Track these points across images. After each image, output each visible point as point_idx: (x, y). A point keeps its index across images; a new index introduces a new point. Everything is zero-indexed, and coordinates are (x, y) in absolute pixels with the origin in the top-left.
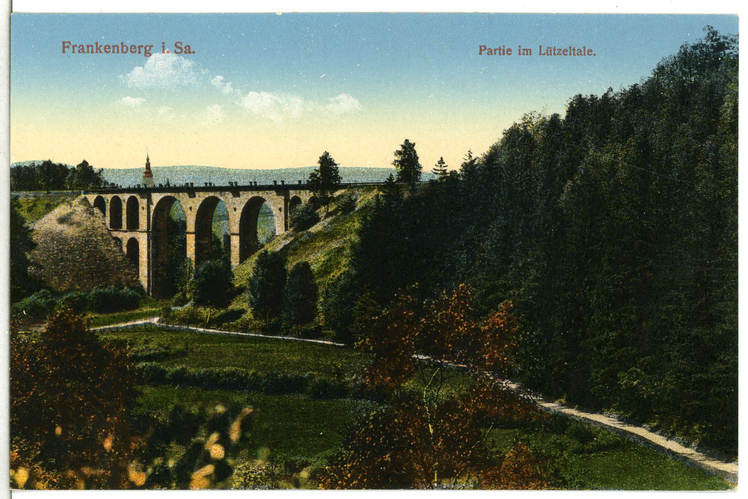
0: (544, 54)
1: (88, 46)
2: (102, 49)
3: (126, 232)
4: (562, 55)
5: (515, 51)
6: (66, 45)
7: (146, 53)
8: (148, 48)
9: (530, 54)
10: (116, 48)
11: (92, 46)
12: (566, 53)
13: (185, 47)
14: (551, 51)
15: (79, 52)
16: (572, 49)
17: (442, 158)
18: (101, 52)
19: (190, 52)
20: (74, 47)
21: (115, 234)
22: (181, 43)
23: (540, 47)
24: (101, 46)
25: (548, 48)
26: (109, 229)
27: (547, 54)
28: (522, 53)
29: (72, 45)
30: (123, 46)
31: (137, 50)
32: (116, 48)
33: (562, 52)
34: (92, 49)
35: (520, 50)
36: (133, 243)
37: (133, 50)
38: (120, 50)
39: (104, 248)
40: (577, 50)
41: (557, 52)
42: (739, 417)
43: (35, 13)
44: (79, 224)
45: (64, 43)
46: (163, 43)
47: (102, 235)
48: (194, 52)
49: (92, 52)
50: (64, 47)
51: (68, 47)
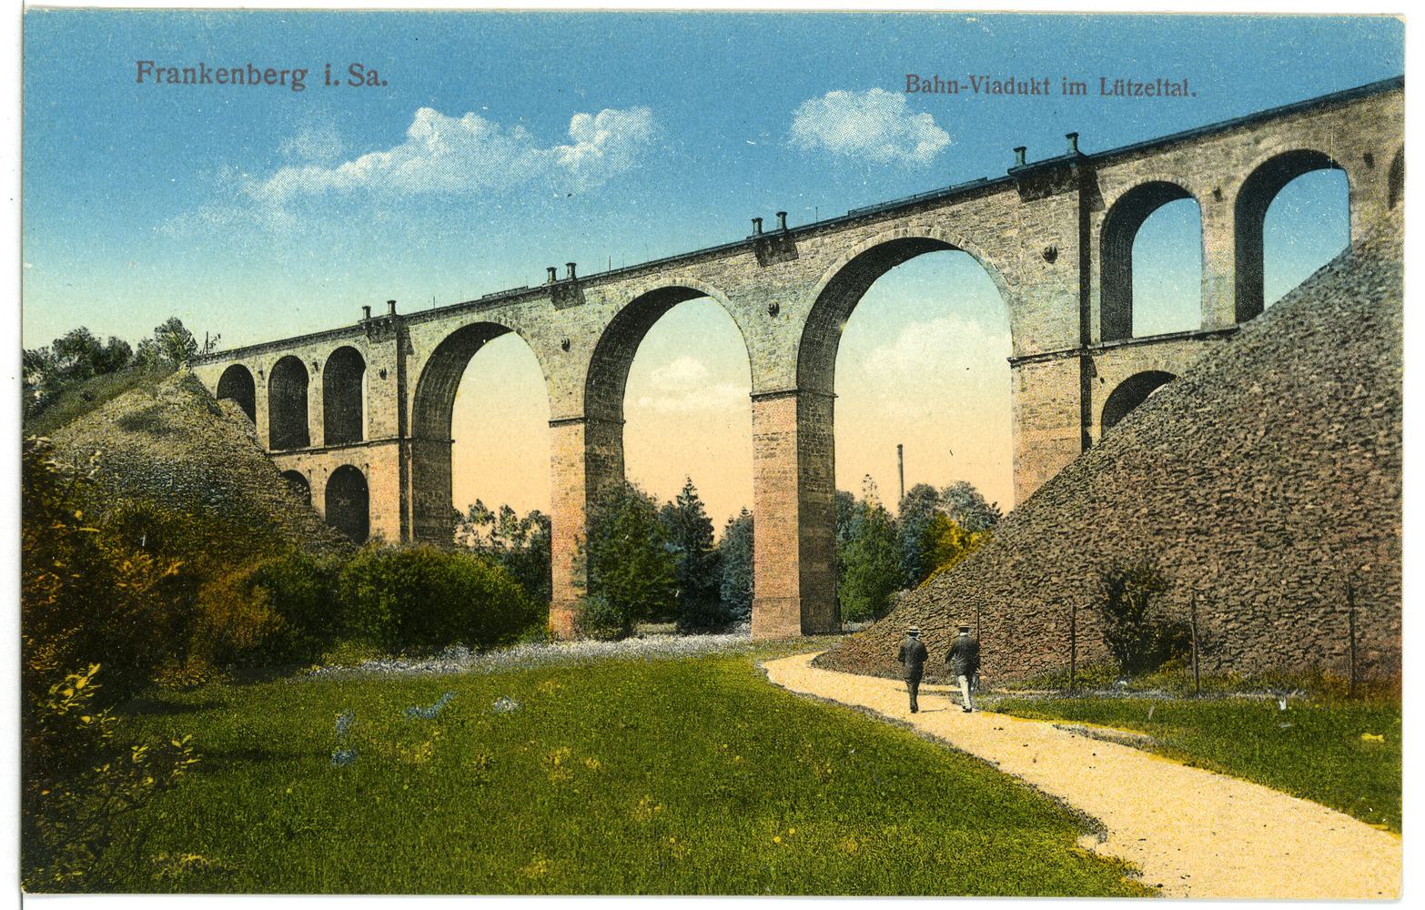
0: (1110, 94)
1: (186, 71)
2: (212, 76)
3: (324, 451)
7: (295, 83)
9: (1085, 93)
11: (193, 70)
14: (1122, 86)
16: (1163, 82)
18: (210, 81)
19: (377, 84)
20: (159, 71)
21: (286, 462)
24: (210, 70)
25: (1117, 81)
26: (268, 451)
27: (1116, 91)
32: (190, 74)
33: (1143, 89)
34: (194, 74)
35: (1064, 85)
36: (350, 484)
39: (261, 498)
41: (1133, 90)
42: (1309, 808)
44: (182, 434)
45: (140, 64)
47: (251, 464)
48: (385, 83)
49: (194, 81)
50: (141, 71)
51: (148, 72)
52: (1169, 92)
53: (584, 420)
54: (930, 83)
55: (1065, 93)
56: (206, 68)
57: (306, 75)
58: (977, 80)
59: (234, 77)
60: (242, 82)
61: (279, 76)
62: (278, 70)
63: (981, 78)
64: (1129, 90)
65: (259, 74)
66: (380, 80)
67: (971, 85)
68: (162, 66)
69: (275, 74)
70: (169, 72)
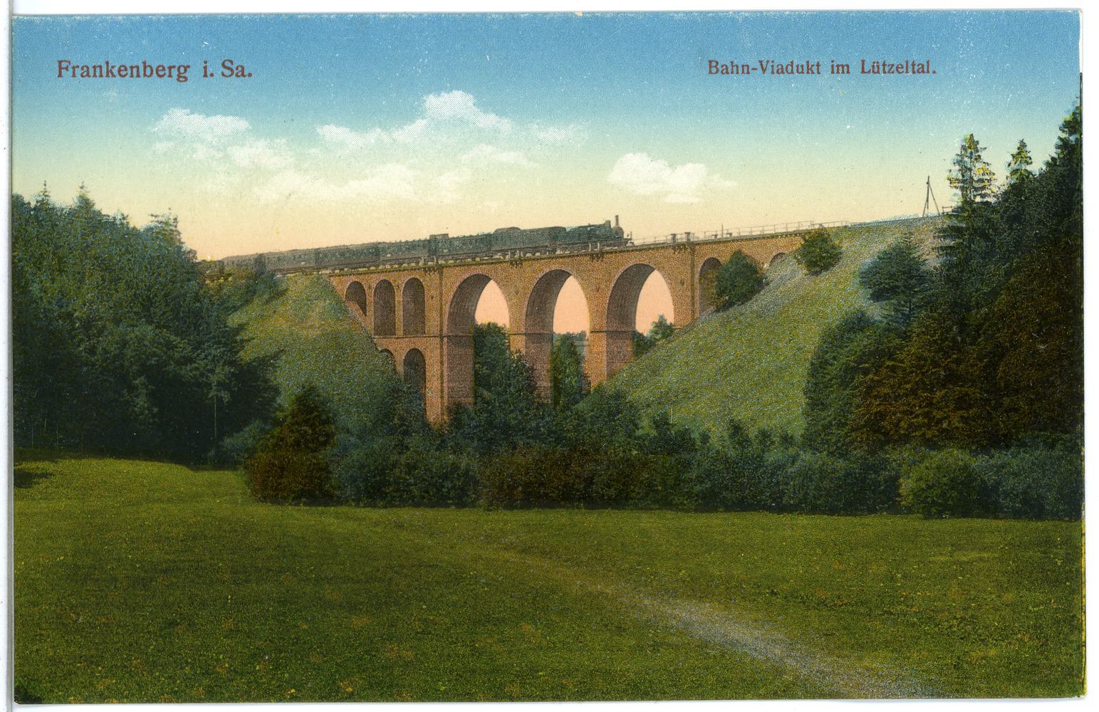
2: (115, 71)
5: (826, 68)
8: (182, 70)
9: (848, 72)
10: (135, 70)
12: (900, 70)
13: (237, 69)
14: (878, 66)
18: (114, 76)
19: (243, 75)
20: (74, 68)
21: (383, 343)
22: (231, 62)
24: (113, 67)
25: (874, 63)
28: (835, 71)
29: (72, 65)
31: (167, 71)
32: (98, 69)
33: (895, 67)
34: (138, 71)
35: (833, 66)
36: (416, 360)
38: (142, 73)
40: (918, 66)
43: (445, 14)
45: (60, 62)
46: (206, 62)
48: (250, 75)
50: (60, 68)
51: (67, 69)
53: (525, 334)
54: (923, 66)
55: (833, 72)
56: (110, 66)
57: (188, 70)
58: (764, 64)
60: (737, 73)
62: (166, 66)
63: (768, 62)
64: (884, 69)
65: (152, 70)
66: (246, 73)
67: (760, 68)
69: (126, 69)
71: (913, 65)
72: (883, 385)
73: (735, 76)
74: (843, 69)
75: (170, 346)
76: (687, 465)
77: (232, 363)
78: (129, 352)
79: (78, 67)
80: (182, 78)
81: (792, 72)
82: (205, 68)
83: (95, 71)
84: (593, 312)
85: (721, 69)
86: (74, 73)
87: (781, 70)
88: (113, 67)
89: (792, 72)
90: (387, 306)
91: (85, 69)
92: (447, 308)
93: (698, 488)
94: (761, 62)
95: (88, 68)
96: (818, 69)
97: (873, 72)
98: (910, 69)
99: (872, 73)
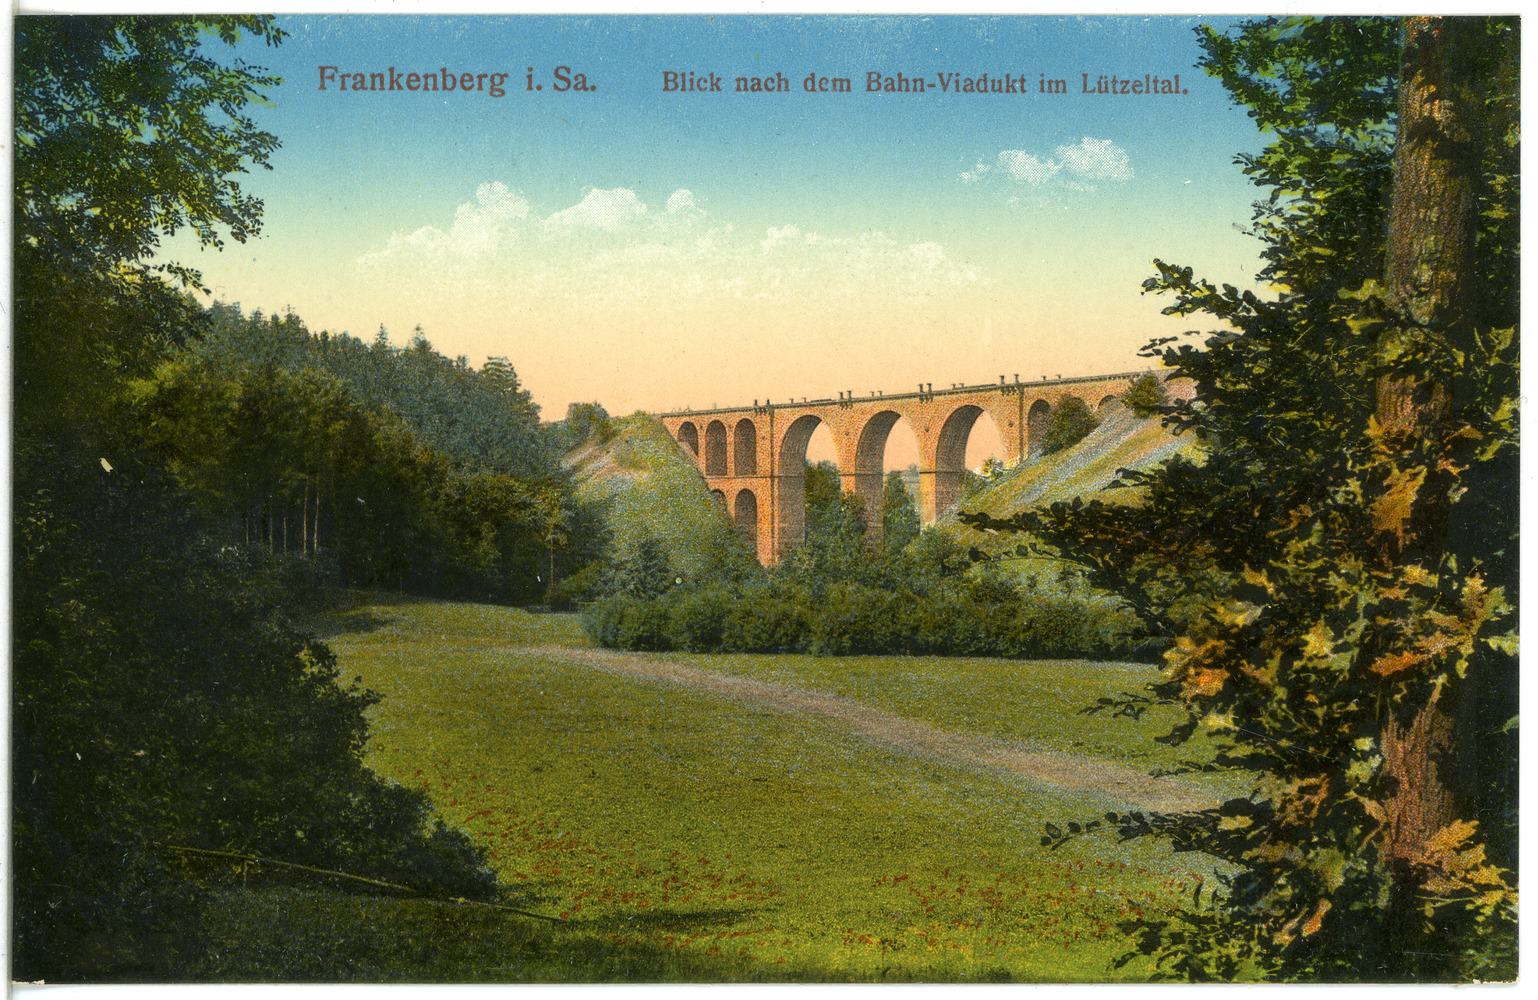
1: (915, 81)
2: (403, 81)
4: (1131, 93)
6: (328, 72)
8: (497, 80)
11: (435, 76)
13: (576, 78)
15: (354, 87)
16: (1151, 80)
17: (1261, 257)
18: (400, 87)
19: (585, 89)
20: (343, 77)
21: (714, 483)
23: (1085, 76)
24: (400, 75)
30: (900, 81)
32: (377, 80)
33: (1129, 87)
34: (435, 81)
35: (1042, 82)
36: (747, 498)
37: (467, 84)
45: (322, 69)
48: (593, 88)
51: (332, 77)
52: (1159, 89)
54: (1169, 83)
55: (1042, 90)
59: (426, 84)
61: (476, 80)
63: (951, 74)
64: (1156, 88)
65: (454, 79)
66: (588, 85)
67: (938, 82)
68: (345, 71)
69: (471, 79)
70: (355, 78)
71: (1155, 81)
72: (1417, 589)
73: (904, 95)
74: (1057, 86)
75: (510, 490)
76: (1013, 614)
77: (568, 507)
78: (469, 499)
79: (349, 75)
80: (497, 91)
81: (813, 90)
82: (530, 77)
83: (1050, 86)
84: (924, 449)
85: (884, 84)
86: (343, 83)
87: (970, 86)
88: (1015, 81)
89: (986, 90)
90: (718, 448)
91: (359, 78)
92: (777, 450)
93: (1022, 637)
94: (940, 75)
95: (363, 77)
96: (1022, 87)
97: (1100, 92)
98: (1152, 89)
99: (1096, 94)
